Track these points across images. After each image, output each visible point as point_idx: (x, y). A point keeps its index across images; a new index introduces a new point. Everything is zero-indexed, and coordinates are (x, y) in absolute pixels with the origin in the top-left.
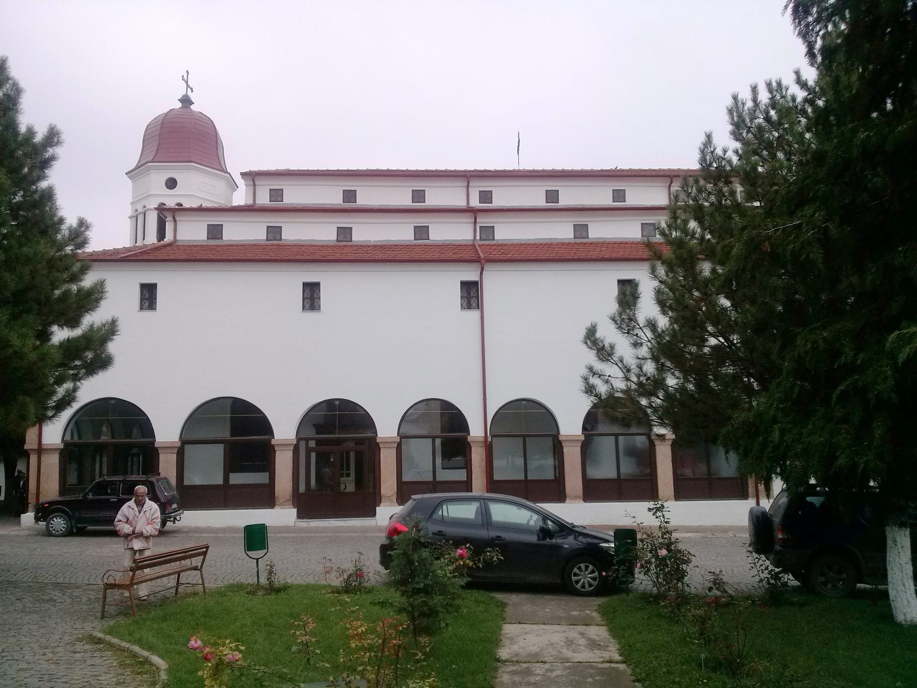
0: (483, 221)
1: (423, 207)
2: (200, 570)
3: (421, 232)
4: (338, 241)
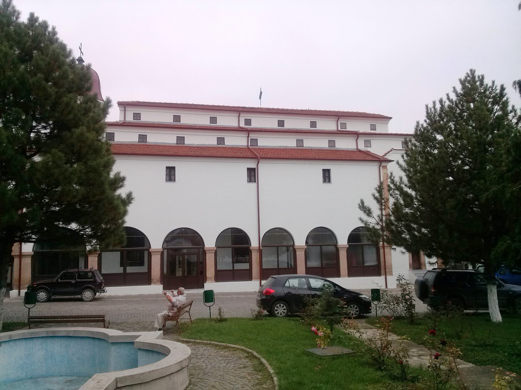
0: (253, 136)
1: (139, 123)
2: (189, 312)
3: (143, 138)
4: (177, 144)
